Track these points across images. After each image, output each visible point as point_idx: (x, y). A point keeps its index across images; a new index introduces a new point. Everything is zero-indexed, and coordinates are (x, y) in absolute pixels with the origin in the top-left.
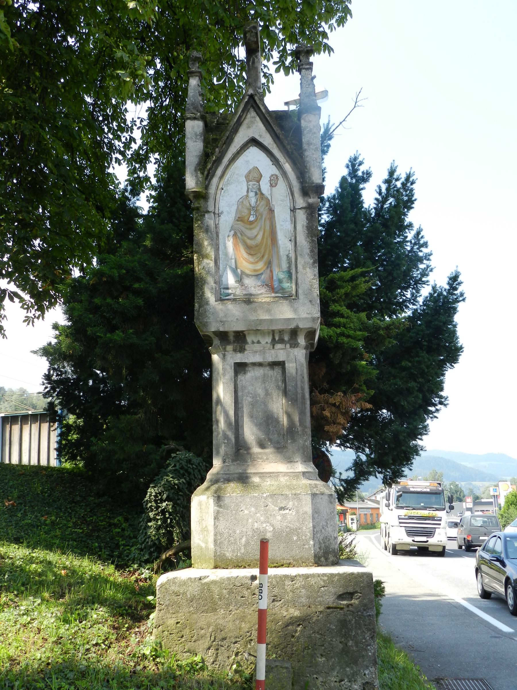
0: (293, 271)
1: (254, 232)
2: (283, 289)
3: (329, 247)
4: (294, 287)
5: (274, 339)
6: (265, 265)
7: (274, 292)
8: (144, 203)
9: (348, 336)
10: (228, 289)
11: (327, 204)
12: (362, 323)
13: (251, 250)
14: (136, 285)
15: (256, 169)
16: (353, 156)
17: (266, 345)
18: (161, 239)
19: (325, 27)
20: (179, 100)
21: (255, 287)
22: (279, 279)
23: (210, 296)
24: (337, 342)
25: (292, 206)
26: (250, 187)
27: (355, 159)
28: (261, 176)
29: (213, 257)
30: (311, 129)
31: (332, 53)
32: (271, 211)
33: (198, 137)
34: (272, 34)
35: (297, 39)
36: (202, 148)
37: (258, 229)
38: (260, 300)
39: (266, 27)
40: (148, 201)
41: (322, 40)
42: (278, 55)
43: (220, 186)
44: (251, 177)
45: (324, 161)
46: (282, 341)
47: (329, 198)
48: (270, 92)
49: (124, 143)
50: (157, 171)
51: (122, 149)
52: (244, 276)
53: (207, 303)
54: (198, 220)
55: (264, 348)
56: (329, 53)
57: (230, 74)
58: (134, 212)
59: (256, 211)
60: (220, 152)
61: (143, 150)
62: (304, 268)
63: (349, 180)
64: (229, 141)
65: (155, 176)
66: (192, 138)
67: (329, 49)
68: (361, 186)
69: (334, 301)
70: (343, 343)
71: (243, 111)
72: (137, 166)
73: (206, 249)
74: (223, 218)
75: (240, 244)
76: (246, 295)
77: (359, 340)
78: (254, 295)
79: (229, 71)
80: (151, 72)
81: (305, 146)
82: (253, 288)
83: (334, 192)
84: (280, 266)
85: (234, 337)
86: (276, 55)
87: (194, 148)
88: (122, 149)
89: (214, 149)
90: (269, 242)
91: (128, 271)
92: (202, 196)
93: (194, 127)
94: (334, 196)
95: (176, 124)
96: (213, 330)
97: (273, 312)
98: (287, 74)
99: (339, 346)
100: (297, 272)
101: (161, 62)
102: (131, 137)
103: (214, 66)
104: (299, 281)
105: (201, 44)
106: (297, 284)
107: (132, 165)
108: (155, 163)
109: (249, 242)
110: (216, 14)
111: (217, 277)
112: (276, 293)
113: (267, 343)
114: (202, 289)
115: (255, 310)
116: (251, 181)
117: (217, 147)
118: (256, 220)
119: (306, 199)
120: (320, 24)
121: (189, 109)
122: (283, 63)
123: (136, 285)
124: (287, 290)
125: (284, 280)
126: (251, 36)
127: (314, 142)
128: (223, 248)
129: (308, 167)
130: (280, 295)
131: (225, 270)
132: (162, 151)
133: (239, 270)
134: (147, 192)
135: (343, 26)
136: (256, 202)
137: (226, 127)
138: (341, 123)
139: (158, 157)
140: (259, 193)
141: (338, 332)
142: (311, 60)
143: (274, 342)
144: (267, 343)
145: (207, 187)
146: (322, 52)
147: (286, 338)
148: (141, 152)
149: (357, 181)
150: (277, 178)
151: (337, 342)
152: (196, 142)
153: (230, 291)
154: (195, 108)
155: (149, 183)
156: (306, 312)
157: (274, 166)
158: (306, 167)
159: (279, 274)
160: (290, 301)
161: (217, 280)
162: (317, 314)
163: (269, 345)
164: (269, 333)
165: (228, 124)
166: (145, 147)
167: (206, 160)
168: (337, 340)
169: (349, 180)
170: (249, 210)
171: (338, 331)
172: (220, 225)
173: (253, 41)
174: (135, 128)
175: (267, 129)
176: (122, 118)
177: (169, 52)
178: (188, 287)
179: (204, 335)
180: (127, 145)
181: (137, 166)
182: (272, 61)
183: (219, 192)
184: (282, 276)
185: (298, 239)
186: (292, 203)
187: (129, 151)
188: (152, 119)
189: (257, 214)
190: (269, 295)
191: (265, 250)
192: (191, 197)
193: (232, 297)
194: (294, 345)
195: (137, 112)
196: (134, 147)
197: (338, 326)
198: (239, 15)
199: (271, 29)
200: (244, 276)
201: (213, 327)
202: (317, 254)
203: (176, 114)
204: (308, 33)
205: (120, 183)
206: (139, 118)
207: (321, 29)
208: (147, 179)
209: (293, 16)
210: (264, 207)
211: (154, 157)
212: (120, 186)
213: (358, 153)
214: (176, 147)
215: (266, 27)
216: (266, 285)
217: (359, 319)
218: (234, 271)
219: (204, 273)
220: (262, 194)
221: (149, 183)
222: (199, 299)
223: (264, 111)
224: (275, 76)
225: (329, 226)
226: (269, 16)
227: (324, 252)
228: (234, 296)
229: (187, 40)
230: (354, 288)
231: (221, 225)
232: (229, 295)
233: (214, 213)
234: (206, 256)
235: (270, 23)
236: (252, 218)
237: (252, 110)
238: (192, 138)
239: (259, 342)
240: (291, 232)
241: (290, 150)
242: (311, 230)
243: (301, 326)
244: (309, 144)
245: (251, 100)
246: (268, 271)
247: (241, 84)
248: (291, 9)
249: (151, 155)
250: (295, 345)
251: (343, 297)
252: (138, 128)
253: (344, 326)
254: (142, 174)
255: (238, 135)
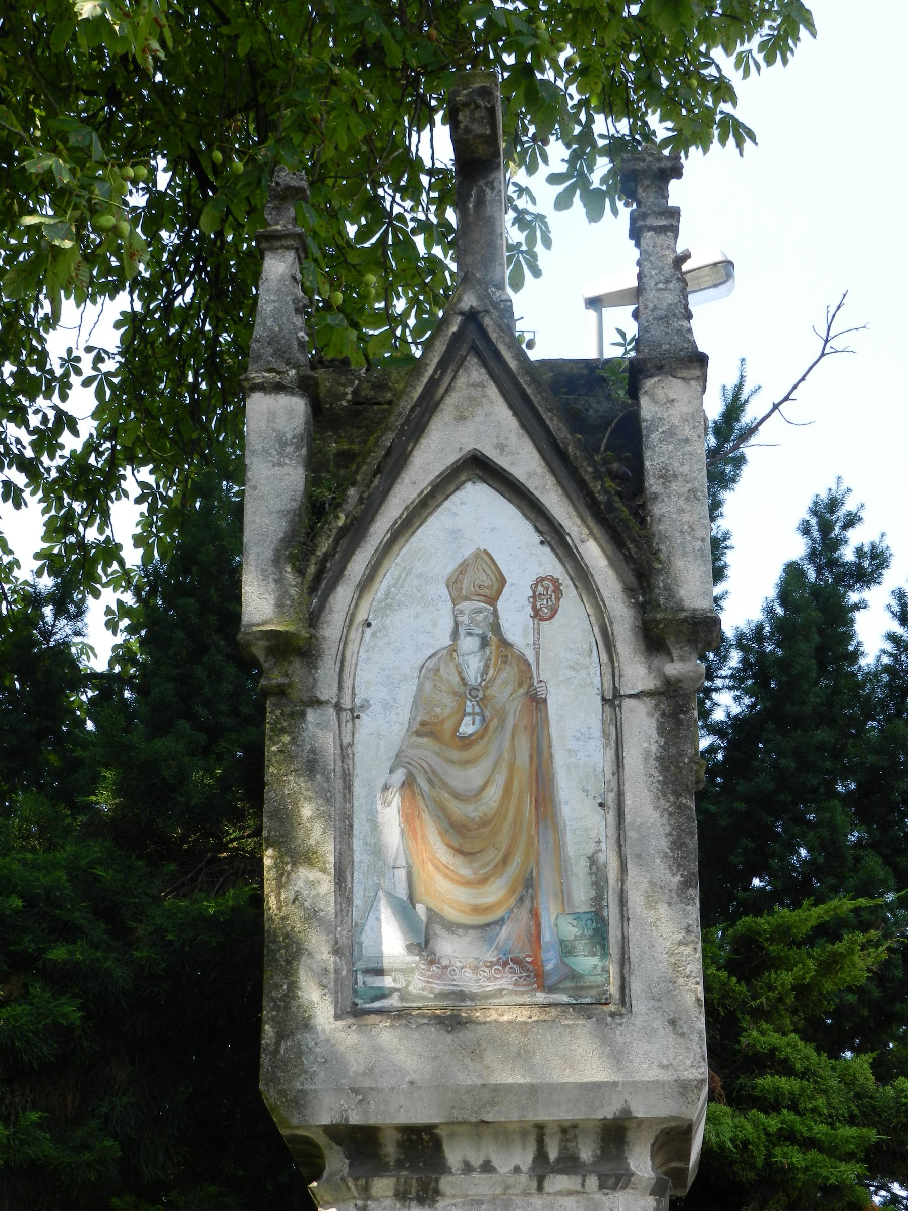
0: (612, 914)
1: (475, 776)
2: (574, 976)
3: (741, 806)
4: (613, 970)
5: (541, 1156)
6: (512, 890)
7: (542, 987)
8: (98, 637)
9: (809, 1144)
10: (380, 972)
11: (735, 658)
12: (857, 1096)
13: (465, 837)
14: (58, 953)
15: (485, 557)
16: (824, 496)
17: (513, 1179)
18: (150, 789)
19: (722, 61)
20: (229, 294)
21: (476, 969)
22: (562, 942)
23: (317, 1002)
24: (768, 1163)
25: (608, 685)
26: (465, 619)
27: (834, 504)
28: (503, 582)
29: (331, 859)
30: (673, 426)
31: (748, 143)
32: (537, 702)
33: (290, 449)
34: (543, 94)
35: (628, 103)
36: (301, 487)
37: (486, 765)
38: (493, 1016)
39: (524, 72)
40: (112, 625)
41: (716, 104)
42: (566, 154)
43: (361, 616)
44: (466, 585)
45: (724, 509)
46: (569, 1163)
47: (740, 636)
48: (537, 273)
49: (36, 431)
50: (147, 523)
51: (29, 453)
52: (438, 928)
53: (306, 1025)
54: (283, 730)
55: (507, 1187)
56: (739, 144)
57: (400, 217)
58: (62, 668)
59: (483, 702)
60: (361, 500)
61: (100, 454)
62: (651, 904)
63: (812, 575)
64: (395, 463)
65: (138, 541)
66: (266, 452)
67: (738, 132)
68: (853, 597)
69: (759, 1014)
70: (792, 1167)
71: (443, 365)
72: (78, 507)
73: (308, 831)
74: (367, 725)
75: (426, 817)
76: (444, 995)
77: (849, 1157)
78: (472, 997)
79: (397, 210)
80: (138, 200)
81: (653, 484)
82: (468, 974)
83: (757, 616)
84: (564, 896)
85: (400, 1145)
86: (557, 152)
87: (271, 487)
88: (29, 453)
89: (342, 489)
90: (528, 811)
91: (30, 901)
92: (297, 648)
93: (273, 417)
94: (760, 627)
95: (213, 370)
96: (325, 1119)
97: (537, 1059)
98: (594, 214)
99: (774, 1178)
100: (624, 918)
101: (173, 167)
102: (60, 414)
103: (348, 193)
104: (634, 951)
105: (305, 125)
106: (624, 960)
107: (60, 506)
108: (138, 501)
109: (457, 809)
110: (359, 27)
111: (342, 933)
112: (551, 990)
113: (517, 1170)
114: (289, 970)
115: (476, 1052)
116: (467, 599)
117: (354, 484)
118: (481, 735)
119: (656, 662)
120: (707, 55)
121: (259, 356)
122: (583, 181)
123: (58, 953)
124: (590, 980)
125: (581, 946)
126: (473, 119)
127: (685, 469)
128: (367, 827)
129: (663, 556)
130: (565, 998)
131: (371, 905)
132: (164, 460)
133: (420, 909)
134: (109, 597)
135: (785, 62)
136: (485, 672)
137: (389, 412)
138: (776, 407)
139: (151, 480)
140: (494, 639)
141: (773, 1129)
142: (672, 202)
143: (542, 1168)
144: (517, 1170)
145: (314, 619)
146: (715, 144)
147: (586, 1153)
148: (92, 460)
149: (839, 579)
150: (558, 590)
151: (768, 1163)
152: (280, 464)
153: (388, 982)
154: (280, 353)
155: (115, 566)
156: (657, 1062)
157: (547, 549)
158: (656, 553)
159: (560, 924)
160: (601, 1021)
161: (343, 941)
162: (693, 1064)
163: (523, 1179)
164: (524, 1135)
165: (390, 403)
166: (108, 444)
167: (312, 528)
168: (769, 1155)
169: (812, 575)
170: (460, 697)
171: (773, 1123)
172: (359, 749)
173: (482, 136)
174: (74, 380)
175: (523, 425)
176: (33, 350)
177: (200, 137)
178: (238, 969)
179: (295, 1139)
180: (46, 440)
181: (78, 507)
182: (543, 171)
183: (355, 635)
184: (570, 930)
185: (629, 802)
186: (608, 678)
187: (52, 457)
188: (136, 352)
189: (485, 712)
190: (527, 999)
191: (514, 839)
192: (259, 651)
193: (394, 1002)
194: (616, 1179)
195: (87, 329)
196: (70, 443)
197: (771, 1105)
198: (434, 33)
199: (539, 76)
200: (438, 928)
201: (326, 1110)
202: (694, 856)
203: (217, 336)
204: (665, 83)
205: (16, 563)
206: (89, 349)
207: (712, 71)
208: (110, 551)
209: (611, 35)
210: (510, 688)
211: (136, 478)
212: (16, 572)
213: (843, 488)
214: (212, 441)
215: (524, 72)
216: (516, 961)
217: (847, 1079)
218: (405, 910)
219: (297, 923)
220: (505, 644)
221: (115, 566)
222: (276, 1008)
223: (513, 364)
224: (554, 219)
225: (737, 731)
226: (535, 35)
227: (723, 822)
228: (402, 998)
229: (262, 99)
230: (829, 966)
231: (359, 749)
232: (383, 994)
233: (338, 707)
234: (308, 857)
235: (537, 57)
236: (468, 727)
237: (472, 361)
238: (266, 452)
239: (487, 1167)
240: (603, 769)
241: (602, 498)
242: (671, 764)
243: (639, 1110)
244: (667, 476)
245: (471, 327)
246: (523, 914)
247: (437, 251)
248: (606, 14)
249: (127, 471)
250: (618, 1179)
251: (791, 999)
252: (87, 383)
253: (794, 1107)
254: (92, 535)
255: (424, 443)
